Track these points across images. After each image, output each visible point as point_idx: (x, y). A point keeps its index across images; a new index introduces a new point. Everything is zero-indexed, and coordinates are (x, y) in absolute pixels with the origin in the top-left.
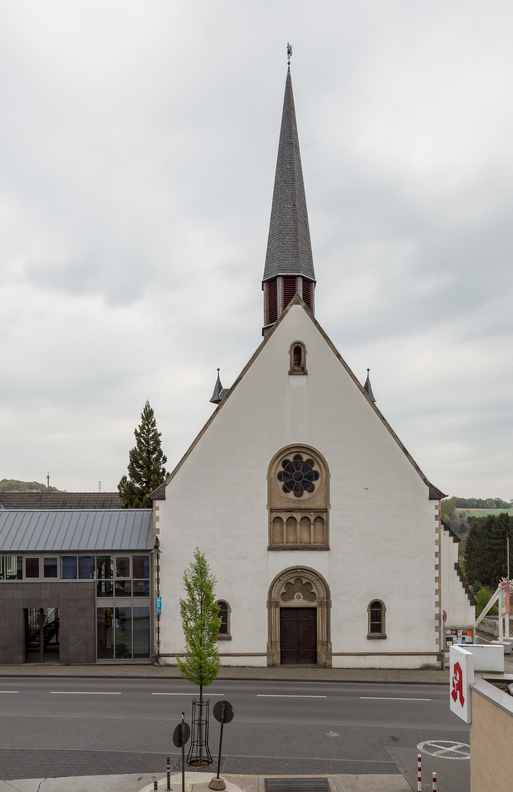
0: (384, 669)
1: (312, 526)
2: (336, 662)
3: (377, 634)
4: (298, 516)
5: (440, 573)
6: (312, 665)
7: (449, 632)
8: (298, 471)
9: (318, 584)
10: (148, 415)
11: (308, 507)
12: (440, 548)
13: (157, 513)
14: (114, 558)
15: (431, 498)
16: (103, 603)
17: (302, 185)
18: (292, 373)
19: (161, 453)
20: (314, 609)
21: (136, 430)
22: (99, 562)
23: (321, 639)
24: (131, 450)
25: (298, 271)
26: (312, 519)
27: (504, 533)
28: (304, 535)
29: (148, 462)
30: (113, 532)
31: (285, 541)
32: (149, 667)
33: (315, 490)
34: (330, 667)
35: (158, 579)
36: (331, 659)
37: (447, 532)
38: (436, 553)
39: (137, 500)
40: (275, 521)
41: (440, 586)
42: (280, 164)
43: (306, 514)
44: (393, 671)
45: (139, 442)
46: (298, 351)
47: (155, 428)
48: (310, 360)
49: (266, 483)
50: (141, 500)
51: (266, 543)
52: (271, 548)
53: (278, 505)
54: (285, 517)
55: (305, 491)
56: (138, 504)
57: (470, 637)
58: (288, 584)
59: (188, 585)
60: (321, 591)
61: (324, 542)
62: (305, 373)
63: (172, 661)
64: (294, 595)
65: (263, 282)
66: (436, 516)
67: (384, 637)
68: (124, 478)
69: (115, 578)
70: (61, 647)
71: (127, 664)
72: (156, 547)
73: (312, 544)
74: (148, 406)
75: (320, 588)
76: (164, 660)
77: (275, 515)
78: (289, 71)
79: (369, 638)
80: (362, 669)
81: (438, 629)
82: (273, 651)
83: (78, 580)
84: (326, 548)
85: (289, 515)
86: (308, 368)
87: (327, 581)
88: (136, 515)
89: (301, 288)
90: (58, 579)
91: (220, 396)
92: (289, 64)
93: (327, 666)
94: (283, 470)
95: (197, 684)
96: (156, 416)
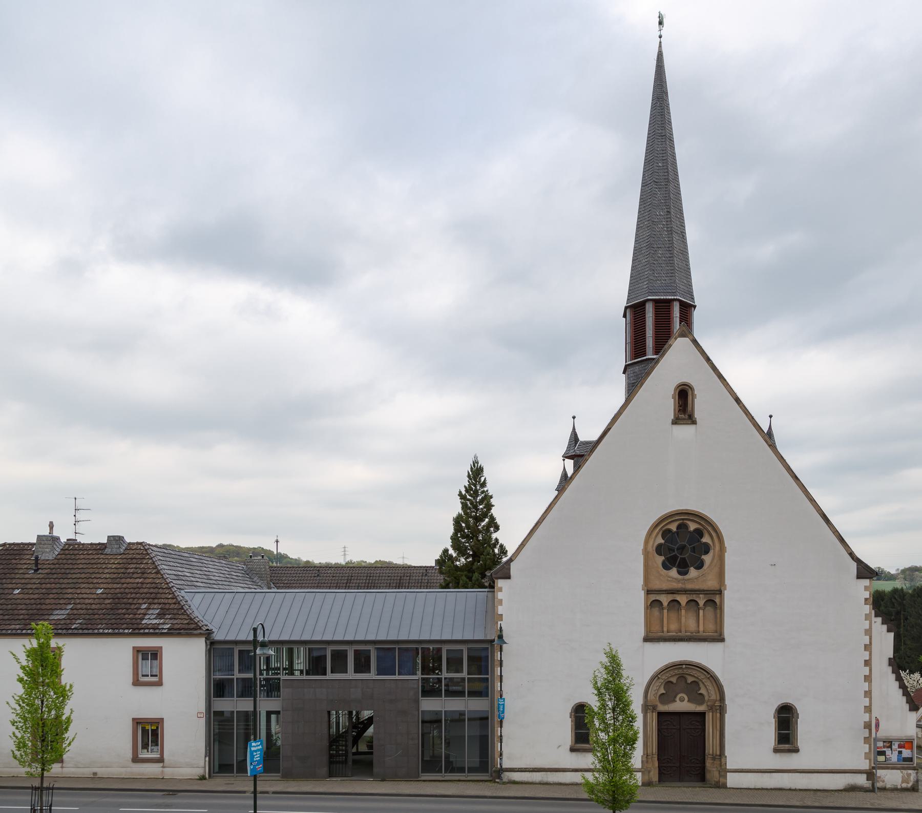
0: (795, 790)
1: (701, 612)
2: (732, 780)
3: (787, 746)
4: (683, 599)
5: (870, 670)
6: (700, 784)
7: (880, 744)
8: (684, 544)
9: (708, 683)
10: (476, 473)
11: (697, 587)
12: (871, 639)
13: (500, 595)
14: (445, 648)
15: (859, 577)
16: (429, 705)
17: (677, 187)
18: (676, 422)
19: (492, 519)
20: (703, 715)
21: (460, 492)
22: (427, 657)
23: (711, 752)
24: (455, 516)
25: (674, 294)
26: (701, 603)
27: (898, 613)
28: (689, 622)
29: (475, 532)
30: (441, 617)
31: (665, 629)
32: (488, 783)
33: (705, 567)
34: (724, 786)
35: (501, 676)
36: (725, 777)
37: (879, 620)
38: (865, 645)
39: (464, 578)
40: (653, 605)
41: (870, 686)
42: (648, 162)
43: (694, 597)
44: (808, 793)
45: (464, 507)
46: (684, 395)
47: (485, 489)
48: (700, 406)
49: (642, 558)
50: (470, 579)
51: (642, 632)
52: (647, 639)
53: (657, 585)
54: (665, 599)
55: (692, 568)
56: (466, 583)
57: (909, 751)
58: (668, 684)
59: (598, 689)
60: (713, 692)
61: (716, 632)
62: (694, 422)
63: (516, 776)
64: (675, 697)
65: (626, 308)
66: (866, 600)
67: (796, 750)
68: (446, 551)
69: (445, 674)
70: (375, 758)
71: (459, 781)
72: (500, 637)
73: (701, 633)
74: (475, 462)
75: (711, 688)
76: (507, 776)
77: (653, 597)
78: (660, 46)
79: (776, 751)
80: (767, 789)
81: (867, 740)
82: (650, 765)
83: (397, 677)
84: (719, 638)
85: (671, 597)
86: (697, 415)
87: (721, 680)
88: (466, 599)
89: (678, 315)
90: (372, 675)
91: (579, 452)
92: (660, 37)
93: (721, 786)
94: (663, 541)
95: (610, 808)
96: (487, 474)
